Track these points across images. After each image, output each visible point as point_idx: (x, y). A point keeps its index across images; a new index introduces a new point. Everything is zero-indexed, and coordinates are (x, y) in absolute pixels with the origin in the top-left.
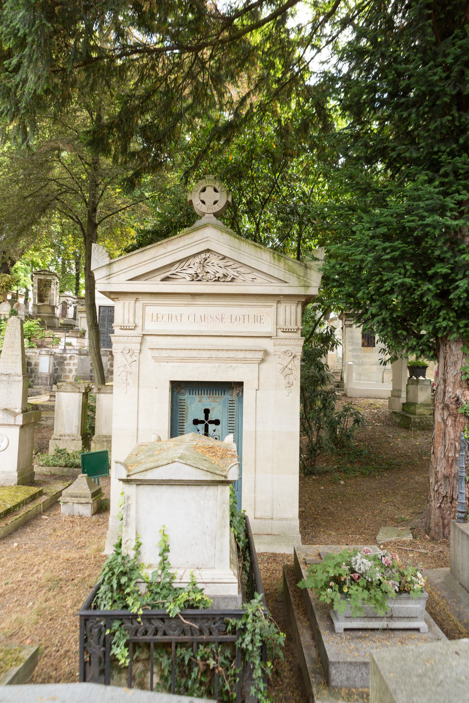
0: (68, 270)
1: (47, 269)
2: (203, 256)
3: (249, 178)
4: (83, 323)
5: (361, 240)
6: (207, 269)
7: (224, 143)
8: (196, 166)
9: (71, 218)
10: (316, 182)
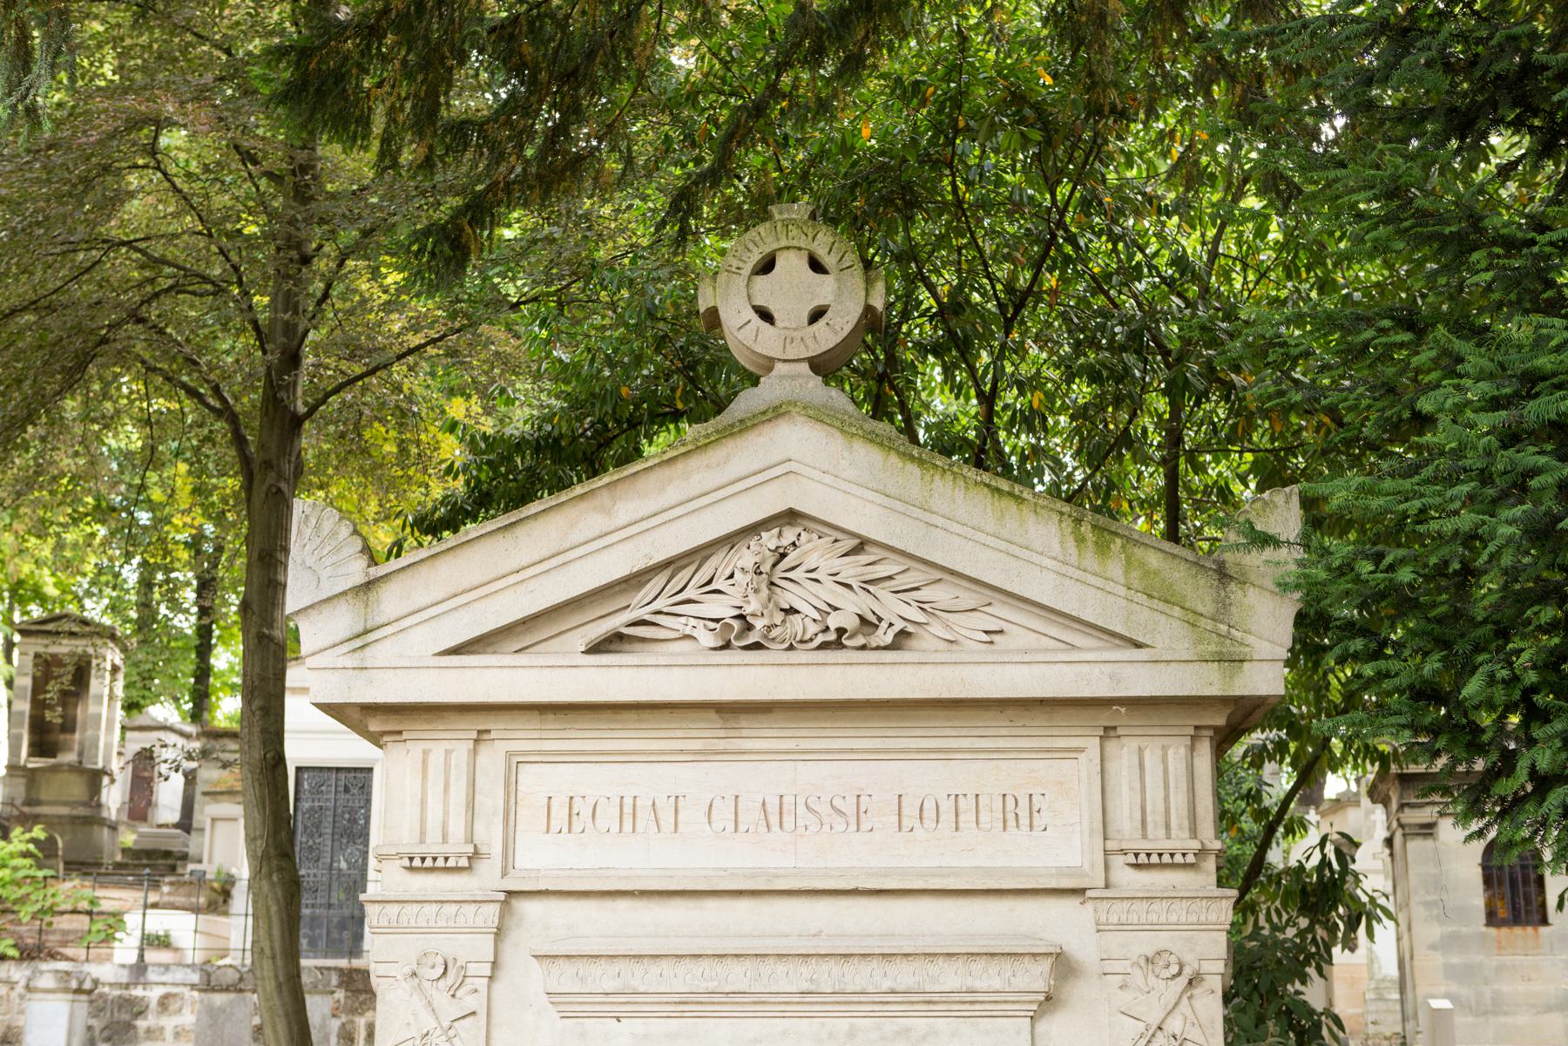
0: (163, 610)
1: (72, 608)
2: (769, 539)
3: (943, 207)
4: (227, 845)
5: (1458, 453)
6: (787, 598)
7: (839, 75)
8: (719, 174)
9: (192, 393)
10: (1225, 217)
